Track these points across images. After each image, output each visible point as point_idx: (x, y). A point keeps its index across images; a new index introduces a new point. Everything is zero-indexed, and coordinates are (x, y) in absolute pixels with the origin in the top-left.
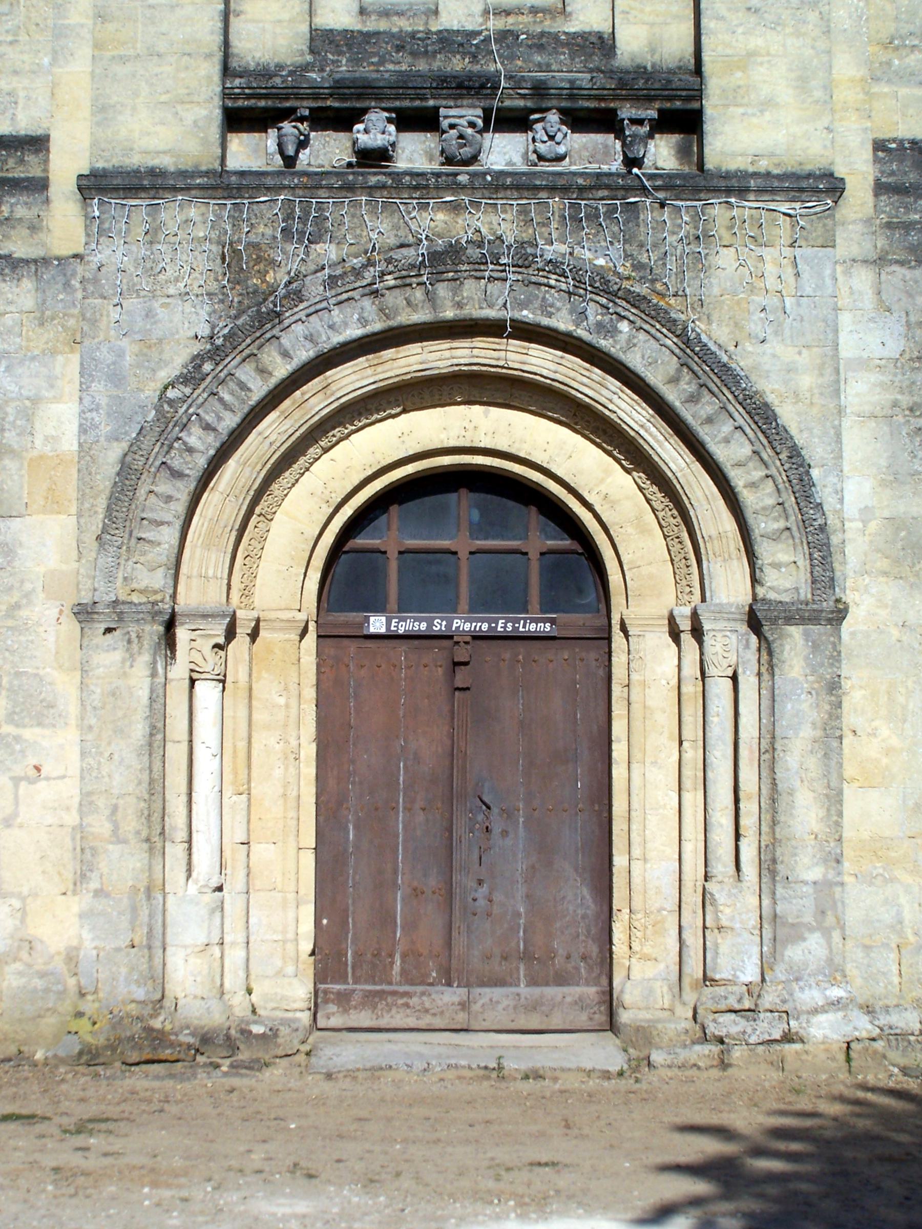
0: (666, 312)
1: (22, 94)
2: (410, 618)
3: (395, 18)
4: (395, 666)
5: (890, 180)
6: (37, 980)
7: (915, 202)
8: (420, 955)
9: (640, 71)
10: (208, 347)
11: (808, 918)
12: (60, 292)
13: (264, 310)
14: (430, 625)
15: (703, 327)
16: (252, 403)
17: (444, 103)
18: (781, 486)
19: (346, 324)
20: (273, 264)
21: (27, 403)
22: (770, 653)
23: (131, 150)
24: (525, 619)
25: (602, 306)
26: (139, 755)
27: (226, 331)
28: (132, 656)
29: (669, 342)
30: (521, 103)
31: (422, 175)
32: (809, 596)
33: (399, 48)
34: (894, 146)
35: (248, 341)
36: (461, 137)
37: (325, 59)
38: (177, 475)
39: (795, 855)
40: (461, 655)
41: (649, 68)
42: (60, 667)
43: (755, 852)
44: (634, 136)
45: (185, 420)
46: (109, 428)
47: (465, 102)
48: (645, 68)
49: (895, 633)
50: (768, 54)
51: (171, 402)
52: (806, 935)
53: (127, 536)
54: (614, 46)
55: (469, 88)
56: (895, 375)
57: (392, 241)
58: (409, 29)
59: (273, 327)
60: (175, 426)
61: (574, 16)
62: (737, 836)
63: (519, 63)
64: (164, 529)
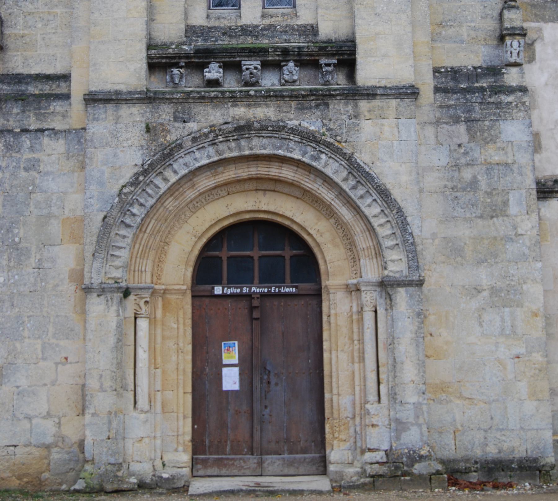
0: (342, 150)
1: (59, 55)
2: (233, 287)
3: (222, 20)
4: (226, 309)
5: (441, 86)
6: (66, 455)
7: (452, 96)
8: (239, 441)
9: (329, 41)
10: (141, 169)
11: (411, 420)
12: (76, 145)
13: (165, 152)
14: (242, 290)
15: (358, 155)
16: (160, 194)
17: (243, 59)
18: (393, 225)
19: (201, 158)
20: (169, 132)
21: (62, 194)
22: (391, 300)
23: (107, 82)
24: (284, 287)
25: (314, 148)
26: (112, 352)
27: (149, 162)
28: (108, 307)
29: (343, 163)
30: (277, 58)
31: (234, 92)
32: (408, 274)
33: (224, 34)
34: (443, 70)
35: (159, 166)
36: (251, 73)
37: (191, 40)
38: (128, 226)
39: (405, 391)
40: (256, 303)
41: (334, 40)
42: (76, 312)
43: (387, 390)
44: (327, 71)
45: (131, 202)
46: (98, 206)
47: (253, 59)
48: (332, 40)
49: (448, 289)
50: (385, 34)
51: (125, 194)
52: (411, 427)
53: (106, 254)
54: (318, 31)
55: (254, 52)
56: (445, 173)
57: (222, 121)
58: (229, 25)
59: (170, 160)
60: (127, 204)
61: (301, 17)
62: (379, 383)
63: (277, 40)
64: (123, 250)
